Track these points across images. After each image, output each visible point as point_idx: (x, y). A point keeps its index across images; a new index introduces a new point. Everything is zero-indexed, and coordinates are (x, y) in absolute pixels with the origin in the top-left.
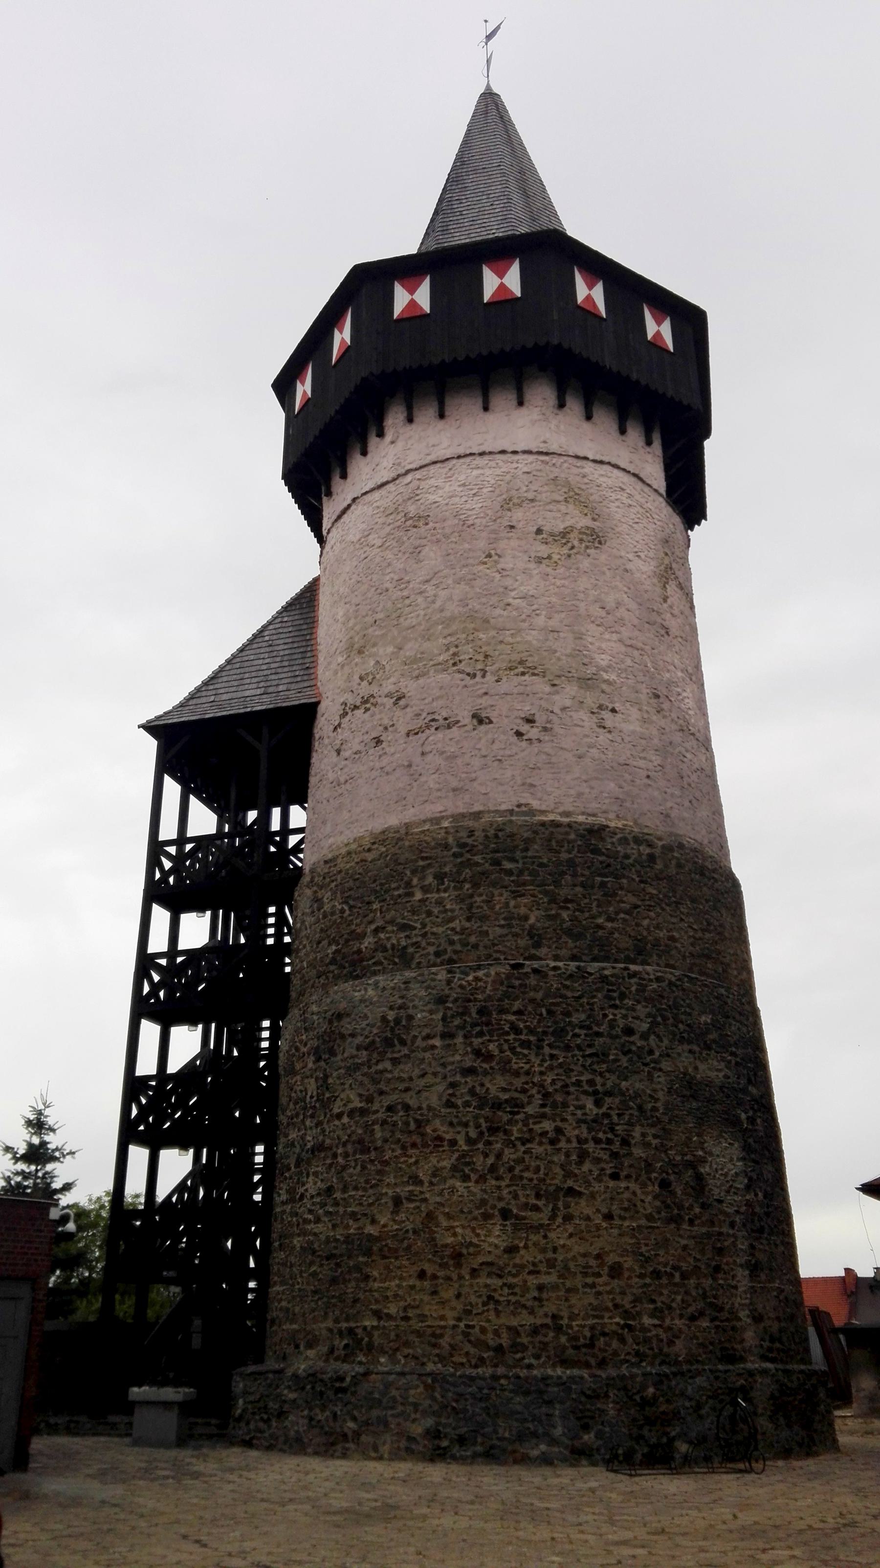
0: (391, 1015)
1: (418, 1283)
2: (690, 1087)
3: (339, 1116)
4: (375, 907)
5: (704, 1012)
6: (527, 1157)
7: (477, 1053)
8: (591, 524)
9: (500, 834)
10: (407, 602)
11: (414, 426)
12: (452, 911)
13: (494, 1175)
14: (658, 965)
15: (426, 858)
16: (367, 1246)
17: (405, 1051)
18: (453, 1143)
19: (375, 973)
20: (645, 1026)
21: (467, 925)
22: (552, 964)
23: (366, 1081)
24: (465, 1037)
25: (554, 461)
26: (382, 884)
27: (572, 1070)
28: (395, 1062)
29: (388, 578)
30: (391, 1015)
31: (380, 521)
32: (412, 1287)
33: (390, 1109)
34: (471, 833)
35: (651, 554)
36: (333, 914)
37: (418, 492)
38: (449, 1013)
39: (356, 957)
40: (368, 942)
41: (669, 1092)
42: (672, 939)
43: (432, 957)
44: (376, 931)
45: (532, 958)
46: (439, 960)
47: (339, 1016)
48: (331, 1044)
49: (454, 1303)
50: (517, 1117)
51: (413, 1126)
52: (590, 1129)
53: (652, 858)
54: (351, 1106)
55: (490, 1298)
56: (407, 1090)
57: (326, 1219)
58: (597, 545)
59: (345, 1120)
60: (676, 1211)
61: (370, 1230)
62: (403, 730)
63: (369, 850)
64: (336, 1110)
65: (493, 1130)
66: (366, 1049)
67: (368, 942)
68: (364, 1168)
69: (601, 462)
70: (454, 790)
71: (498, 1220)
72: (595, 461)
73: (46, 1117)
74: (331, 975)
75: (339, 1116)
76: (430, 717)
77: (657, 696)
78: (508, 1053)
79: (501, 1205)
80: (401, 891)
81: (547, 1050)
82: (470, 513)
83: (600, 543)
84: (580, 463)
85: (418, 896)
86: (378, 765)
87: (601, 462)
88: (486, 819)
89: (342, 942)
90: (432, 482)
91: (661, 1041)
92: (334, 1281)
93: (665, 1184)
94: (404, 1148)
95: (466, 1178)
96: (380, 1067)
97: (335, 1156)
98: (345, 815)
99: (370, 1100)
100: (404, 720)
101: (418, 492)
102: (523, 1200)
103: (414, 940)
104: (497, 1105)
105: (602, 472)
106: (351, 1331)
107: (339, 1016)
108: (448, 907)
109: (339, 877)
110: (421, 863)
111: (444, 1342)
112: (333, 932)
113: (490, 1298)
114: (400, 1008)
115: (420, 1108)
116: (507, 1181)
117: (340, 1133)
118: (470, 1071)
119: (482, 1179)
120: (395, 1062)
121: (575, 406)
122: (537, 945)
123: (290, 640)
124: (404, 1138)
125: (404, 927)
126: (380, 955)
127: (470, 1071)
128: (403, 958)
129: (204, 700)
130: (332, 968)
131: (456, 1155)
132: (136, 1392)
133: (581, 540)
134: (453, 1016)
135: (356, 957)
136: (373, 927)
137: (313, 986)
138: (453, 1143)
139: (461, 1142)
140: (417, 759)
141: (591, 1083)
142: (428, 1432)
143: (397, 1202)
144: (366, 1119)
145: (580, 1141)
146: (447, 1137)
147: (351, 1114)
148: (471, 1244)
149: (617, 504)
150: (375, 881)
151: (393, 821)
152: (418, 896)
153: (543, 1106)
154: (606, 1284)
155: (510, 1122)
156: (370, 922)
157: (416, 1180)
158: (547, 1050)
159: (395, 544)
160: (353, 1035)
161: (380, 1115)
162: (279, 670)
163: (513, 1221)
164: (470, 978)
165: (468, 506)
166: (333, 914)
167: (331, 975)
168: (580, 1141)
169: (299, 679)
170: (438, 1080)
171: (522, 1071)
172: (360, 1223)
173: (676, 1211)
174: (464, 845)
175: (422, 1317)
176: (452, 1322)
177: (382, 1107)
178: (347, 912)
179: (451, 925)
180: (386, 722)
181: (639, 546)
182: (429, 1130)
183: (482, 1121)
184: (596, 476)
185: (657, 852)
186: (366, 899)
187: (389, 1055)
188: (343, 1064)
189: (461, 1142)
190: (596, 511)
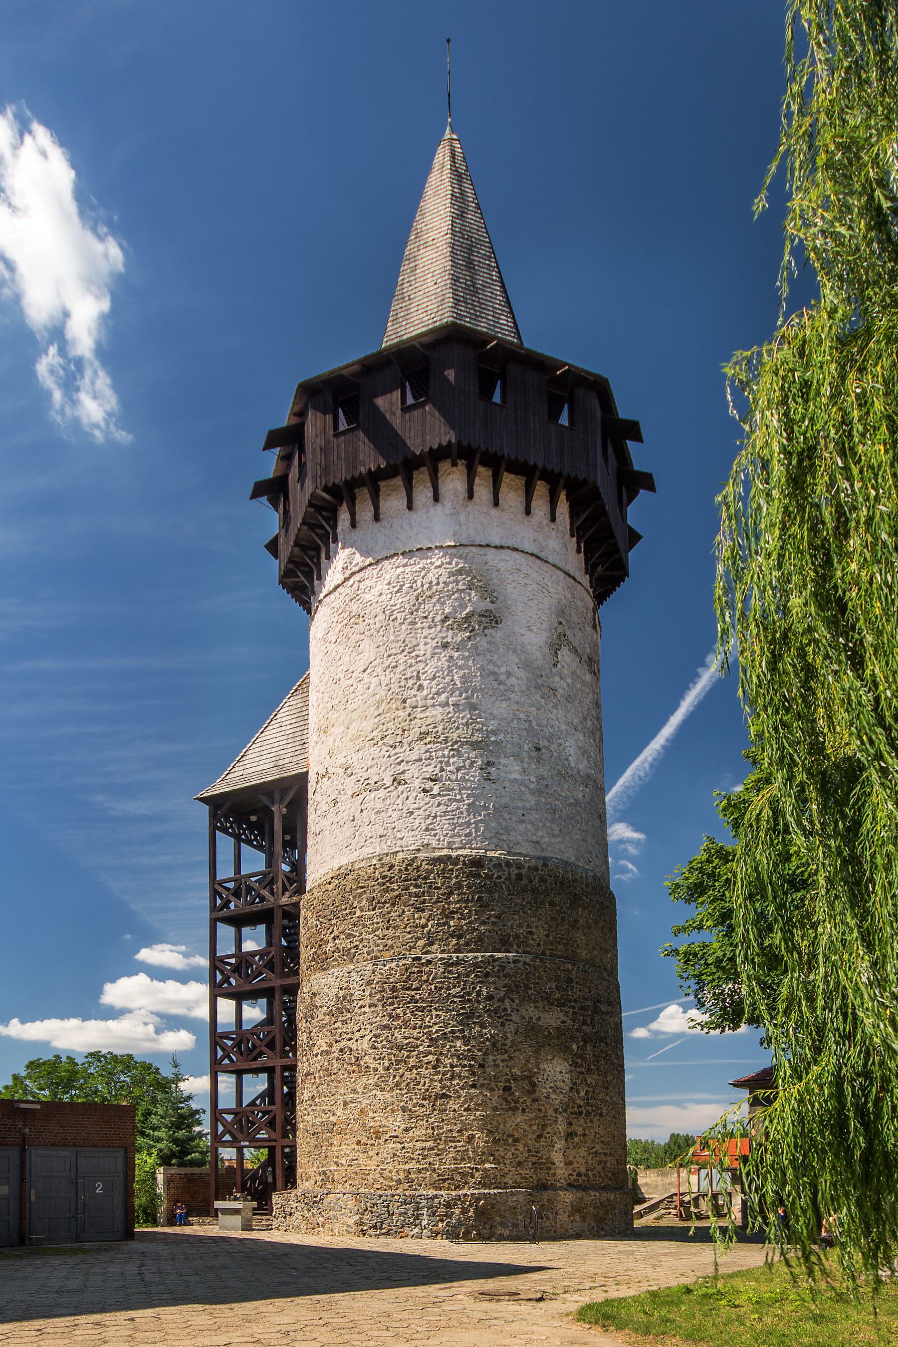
1: (357, 1147)
2: (532, 1030)
3: (316, 1055)
5: (550, 980)
6: (418, 1077)
8: (491, 607)
10: (352, 689)
11: (357, 531)
14: (517, 952)
15: (362, 888)
16: (331, 1128)
17: (349, 1016)
18: (376, 1070)
20: (502, 994)
21: (386, 932)
22: (440, 956)
23: (328, 1034)
24: (383, 1006)
25: (461, 551)
26: (337, 907)
29: (340, 669)
30: (341, 993)
31: (335, 620)
32: (354, 1149)
33: (341, 1050)
34: (391, 867)
35: (544, 626)
36: (312, 928)
37: (358, 592)
38: (374, 991)
40: (330, 947)
41: (516, 1033)
42: (531, 933)
43: (365, 955)
45: (427, 953)
49: (375, 1157)
51: (353, 1060)
52: (459, 1059)
53: (519, 877)
54: (322, 1049)
55: (394, 1155)
56: (351, 1039)
58: (493, 625)
60: (513, 1104)
61: (333, 1119)
62: (350, 793)
64: (315, 1052)
65: (398, 1062)
67: (330, 947)
68: (328, 1085)
69: (502, 547)
70: (381, 837)
72: (496, 547)
75: (316, 1055)
76: (366, 783)
77: (538, 749)
79: (402, 1104)
80: (347, 911)
81: (434, 1013)
82: (394, 608)
83: (497, 623)
84: (483, 551)
86: (335, 821)
87: (502, 547)
88: (400, 856)
90: (367, 582)
91: (513, 1002)
92: (316, 1146)
93: (507, 1089)
94: (349, 1073)
95: (382, 1090)
96: (336, 1025)
97: (315, 1078)
98: (319, 858)
99: (331, 1046)
100: (351, 786)
101: (358, 592)
102: (415, 1101)
103: (355, 944)
104: (400, 1048)
105: (503, 557)
106: (324, 1173)
111: (370, 1177)
113: (394, 1155)
115: (357, 1050)
117: (317, 1065)
118: (386, 1027)
119: (392, 1089)
122: (431, 944)
123: (294, 721)
124: (349, 1067)
125: (349, 936)
127: (386, 1027)
128: (349, 955)
129: (236, 774)
130: (313, 963)
131: (377, 1077)
132: (218, 1204)
133: (480, 623)
134: (375, 993)
136: (332, 936)
138: (376, 1070)
139: (380, 1069)
141: (462, 1031)
142: (356, 1223)
143: (346, 1104)
145: (452, 1066)
146: (372, 1066)
147: (323, 1052)
148: (385, 1126)
149: (514, 584)
151: (344, 861)
152: (358, 913)
154: (463, 1146)
155: (408, 1057)
156: (331, 933)
157: (354, 1091)
158: (434, 1013)
159: (344, 640)
160: (321, 1007)
161: (336, 1055)
162: (285, 747)
164: (386, 968)
165: (392, 602)
168: (452, 1066)
169: (298, 753)
172: (327, 1116)
173: (513, 1104)
174: (384, 877)
175: (359, 1165)
176: (373, 1168)
180: (340, 787)
181: (533, 621)
182: (362, 1063)
184: (496, 562)
185: (524, 872)
186: (329, 917)
187: (340, 1019)
189: (380, 1069)
190: (495, 594)
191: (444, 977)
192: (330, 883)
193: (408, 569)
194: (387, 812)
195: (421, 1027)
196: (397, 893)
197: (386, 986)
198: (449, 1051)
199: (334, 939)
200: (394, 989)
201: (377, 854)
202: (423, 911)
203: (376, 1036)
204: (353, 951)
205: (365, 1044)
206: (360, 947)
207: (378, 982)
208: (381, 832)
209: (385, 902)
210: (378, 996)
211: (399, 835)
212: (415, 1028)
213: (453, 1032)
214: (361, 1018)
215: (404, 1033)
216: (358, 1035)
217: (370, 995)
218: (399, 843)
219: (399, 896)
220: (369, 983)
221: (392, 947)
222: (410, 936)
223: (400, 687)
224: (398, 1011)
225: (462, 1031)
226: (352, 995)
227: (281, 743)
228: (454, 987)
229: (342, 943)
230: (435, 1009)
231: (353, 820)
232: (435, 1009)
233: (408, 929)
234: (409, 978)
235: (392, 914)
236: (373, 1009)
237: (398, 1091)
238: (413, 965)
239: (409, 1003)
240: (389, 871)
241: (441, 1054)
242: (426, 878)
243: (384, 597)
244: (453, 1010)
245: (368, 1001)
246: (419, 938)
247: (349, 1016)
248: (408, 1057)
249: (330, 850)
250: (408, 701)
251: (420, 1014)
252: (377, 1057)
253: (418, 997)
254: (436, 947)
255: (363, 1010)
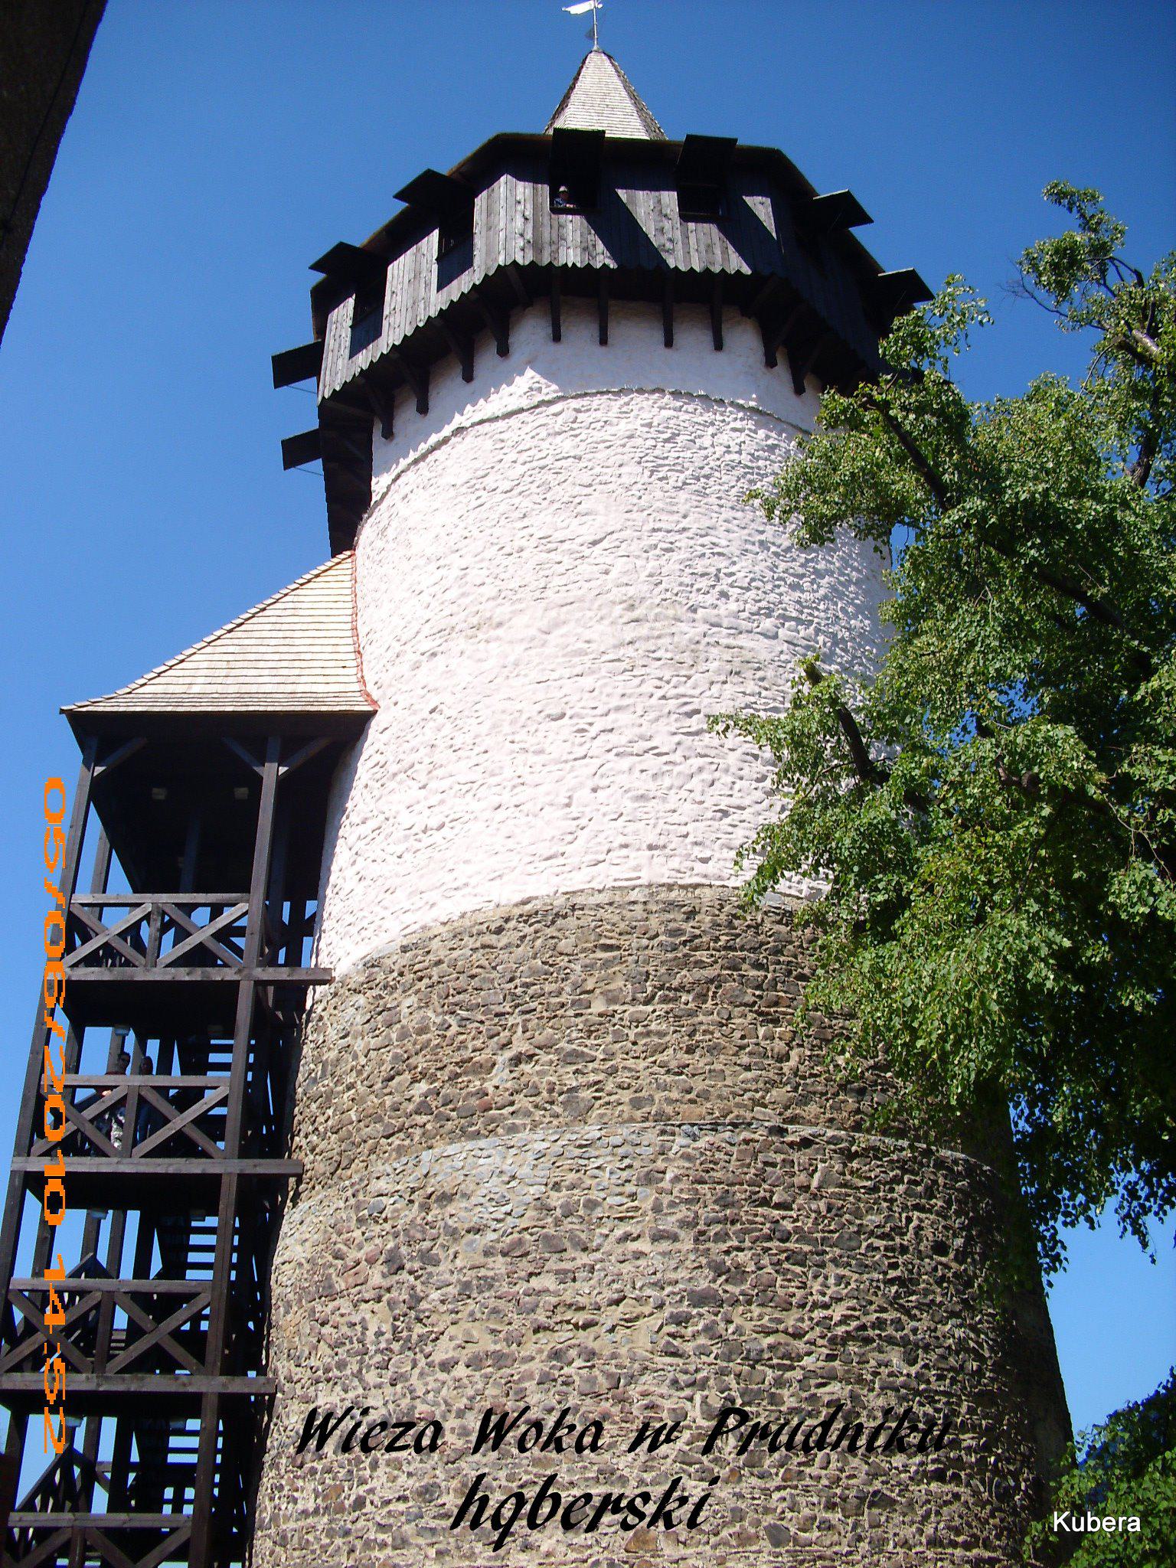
0: (556, 1199)
3: (446, 1366)
4: (511, 1020)
7: (719, 1270)
9: (736, 922)
12: (661, 1034)
13: (756, 1471)
19: (513, 1129)
21: (686, 1058)
27: (871, 1303)
28: (566, 1276)
30: (556, 1199)
33: (556, 1355)
36: (422, 1031)
38: (666, 1200)
39: (474, 1102)
44: (517, 1060)
46: (638, 1114)
47: (446, 1198)
48: (427, 1244)
50: (788, 1375)
51: (603, 1383)
57: (421, 1541)
59: (461, 1371)
63: (499, 931)
66: (504, 1254)
67: (500, 1077)
70: (651, 847)
71: (766, 1544)
73: (1134, 1224)
74: (418, 1131)
78: (770, 1269)
79: (769, 1520)
81: (832, 1271)
85: (599, 1006)
89: (444, 1075)
96: (535, 1283)
102: (806, 1512)
103: (592, 1078)
104: (755, 1360)
107: (446, 1198)
108: (653, 1027)
109: (435, 972)
110: (600, 954)
112: (420, 1062)
114: (573, 1187)
116: (778, 1481)
118: (700, 1299)
120: (566, 1276)
121: (782, 371)
126: (522, 1101)
130: (421, 1119)
134: (672, 1204)
135: (474, 1102)
136: (508, 1054)
137: (372, 1151)
140: (584, 794)
144: (507, 1371)
147: (475, 1363)
150: (512, 980)
152: (599, 1006)
153: (830, 1358)
155: (779, 1383)
156: (504, 1046)
163: (790, 1546)
165: (657, 452)
166: (422, 1031)
167: (418, 1131)
170: (647, 1310)
171: (794, 1301)
177: (540, 1351)
178: (454, 1029)
179: (659, 1058)
182: (633, 1392)
183: (731, 1380)
187: (551, 1265)
188: (454, 1278)
191: (844, 1185)
192: (499, 931)
193: (683, 416)
194: (664, 800)
195: (803, 1306)
196: (710, 973)
197: (704, 1189)
198: (876, 1374)
199: (517, 1060)
200: (724, 1201)
201: (644, 881)
202: (776, 1022)
203: (681, 1320)
204: (587, 1094)
205: (642, 1338)
206: (610, 1086)
207: (677, 1179)
208: (652, 838)
209: (681, 988)
210: (683, 1212)
211: (698, 852)
212: (787, 1307)
213: (880, 1324)
214: (626, 1268)
215: (761, 1317)
216: (616, 1314)
217: (657, 1209)
218: (699, 867)
219: (717, 981)
220: (649, 1179)
221: (705, 1095)
222: (749, 1075)
223: (681, 584)
224: (742, 1257)
225: (898, 1325)
226: (592, 1205)
227: (217, 673)
228: (869, 1210)
229: (540, 1072)
230: (834, 1260)
231: (568, 805)
232: (834, 1260)
233: (745, 1059)
234: (761, 1177)
235: (701, 1018)
236: (665, 1246)
237: (754, 1481)
238: (767, 1146)
239: (769, 1239)
240: (687, 919)
241: (860, 1380)
242: (778, 952)
243: (639, 442)
244: (876, 1266)
245: (646, 1222)
246: (773, 1084)
247: (585, 1259)
248: (779, 1383)
249: (393, 883)
250: (700, 611)
251: (798, 1269)
252: (683, 1378)
253: (788, 1225)
254: (813, 1109)
255: (633, 1246)
